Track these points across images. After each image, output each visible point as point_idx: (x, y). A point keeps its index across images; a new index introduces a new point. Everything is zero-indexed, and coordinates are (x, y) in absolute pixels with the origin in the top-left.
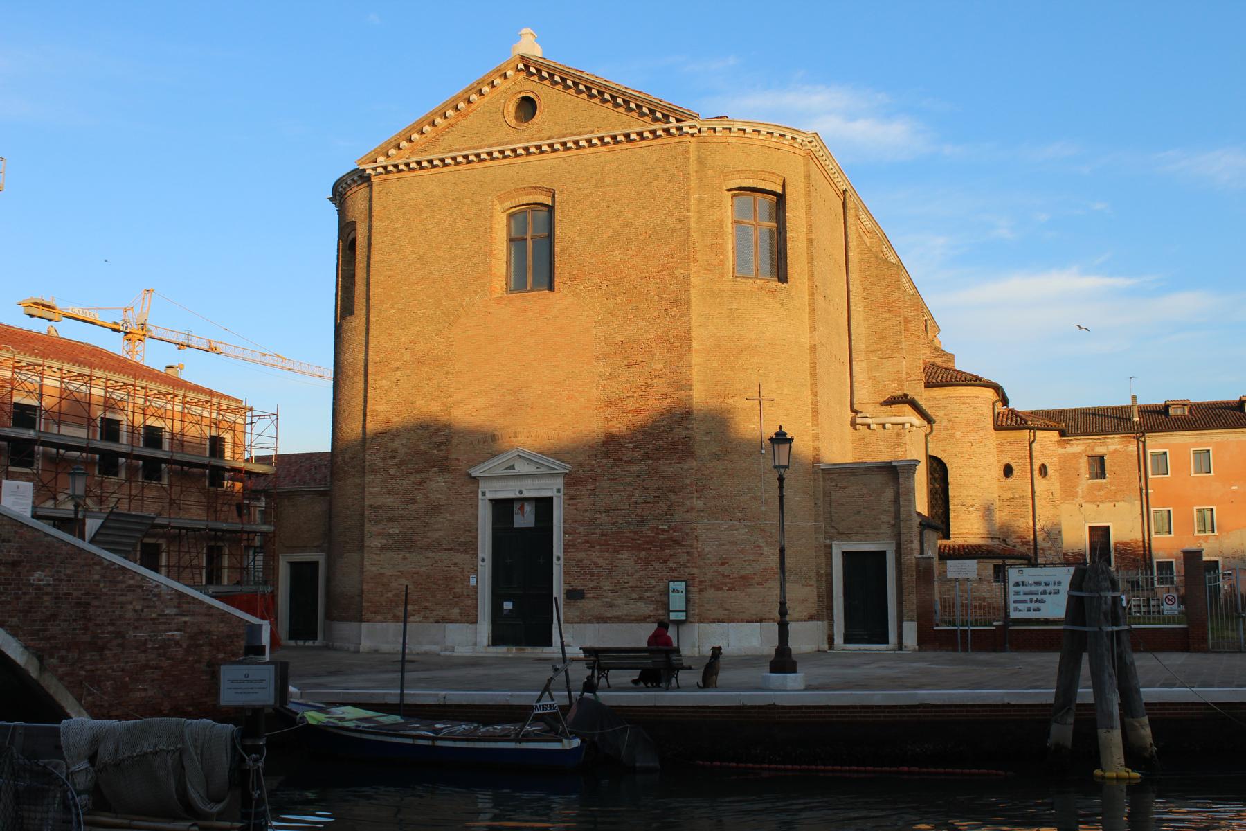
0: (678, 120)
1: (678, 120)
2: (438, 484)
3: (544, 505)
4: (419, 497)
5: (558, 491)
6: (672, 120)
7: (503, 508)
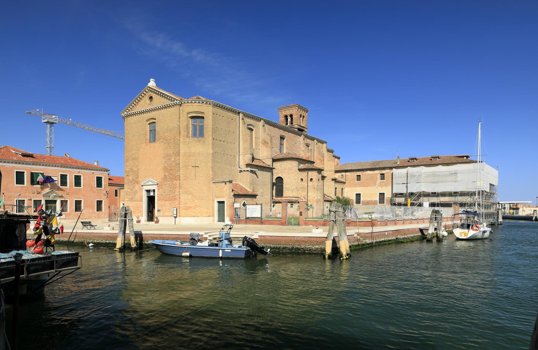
2: (137, 187)
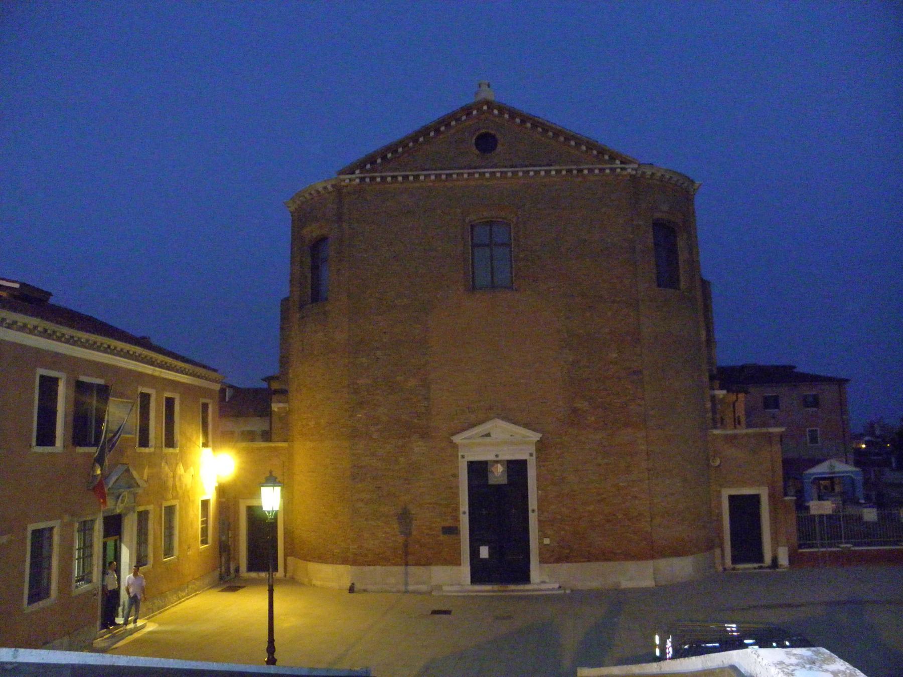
0: (622, 163)
1: (622, 163)
3: (517, 468)
4: (402, 460)
5: (531, 455)
6: (618, 162)
7: (478, 470)
